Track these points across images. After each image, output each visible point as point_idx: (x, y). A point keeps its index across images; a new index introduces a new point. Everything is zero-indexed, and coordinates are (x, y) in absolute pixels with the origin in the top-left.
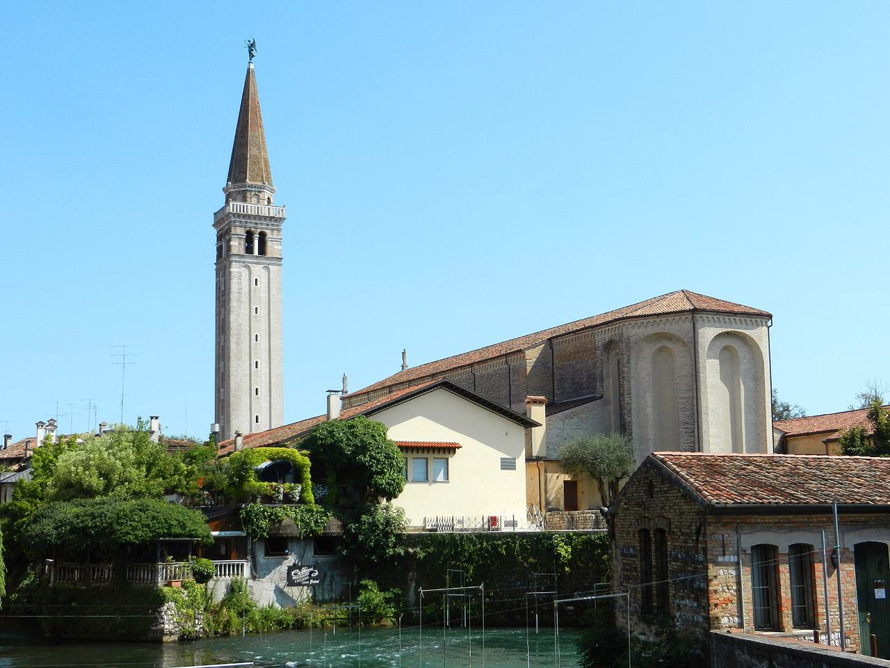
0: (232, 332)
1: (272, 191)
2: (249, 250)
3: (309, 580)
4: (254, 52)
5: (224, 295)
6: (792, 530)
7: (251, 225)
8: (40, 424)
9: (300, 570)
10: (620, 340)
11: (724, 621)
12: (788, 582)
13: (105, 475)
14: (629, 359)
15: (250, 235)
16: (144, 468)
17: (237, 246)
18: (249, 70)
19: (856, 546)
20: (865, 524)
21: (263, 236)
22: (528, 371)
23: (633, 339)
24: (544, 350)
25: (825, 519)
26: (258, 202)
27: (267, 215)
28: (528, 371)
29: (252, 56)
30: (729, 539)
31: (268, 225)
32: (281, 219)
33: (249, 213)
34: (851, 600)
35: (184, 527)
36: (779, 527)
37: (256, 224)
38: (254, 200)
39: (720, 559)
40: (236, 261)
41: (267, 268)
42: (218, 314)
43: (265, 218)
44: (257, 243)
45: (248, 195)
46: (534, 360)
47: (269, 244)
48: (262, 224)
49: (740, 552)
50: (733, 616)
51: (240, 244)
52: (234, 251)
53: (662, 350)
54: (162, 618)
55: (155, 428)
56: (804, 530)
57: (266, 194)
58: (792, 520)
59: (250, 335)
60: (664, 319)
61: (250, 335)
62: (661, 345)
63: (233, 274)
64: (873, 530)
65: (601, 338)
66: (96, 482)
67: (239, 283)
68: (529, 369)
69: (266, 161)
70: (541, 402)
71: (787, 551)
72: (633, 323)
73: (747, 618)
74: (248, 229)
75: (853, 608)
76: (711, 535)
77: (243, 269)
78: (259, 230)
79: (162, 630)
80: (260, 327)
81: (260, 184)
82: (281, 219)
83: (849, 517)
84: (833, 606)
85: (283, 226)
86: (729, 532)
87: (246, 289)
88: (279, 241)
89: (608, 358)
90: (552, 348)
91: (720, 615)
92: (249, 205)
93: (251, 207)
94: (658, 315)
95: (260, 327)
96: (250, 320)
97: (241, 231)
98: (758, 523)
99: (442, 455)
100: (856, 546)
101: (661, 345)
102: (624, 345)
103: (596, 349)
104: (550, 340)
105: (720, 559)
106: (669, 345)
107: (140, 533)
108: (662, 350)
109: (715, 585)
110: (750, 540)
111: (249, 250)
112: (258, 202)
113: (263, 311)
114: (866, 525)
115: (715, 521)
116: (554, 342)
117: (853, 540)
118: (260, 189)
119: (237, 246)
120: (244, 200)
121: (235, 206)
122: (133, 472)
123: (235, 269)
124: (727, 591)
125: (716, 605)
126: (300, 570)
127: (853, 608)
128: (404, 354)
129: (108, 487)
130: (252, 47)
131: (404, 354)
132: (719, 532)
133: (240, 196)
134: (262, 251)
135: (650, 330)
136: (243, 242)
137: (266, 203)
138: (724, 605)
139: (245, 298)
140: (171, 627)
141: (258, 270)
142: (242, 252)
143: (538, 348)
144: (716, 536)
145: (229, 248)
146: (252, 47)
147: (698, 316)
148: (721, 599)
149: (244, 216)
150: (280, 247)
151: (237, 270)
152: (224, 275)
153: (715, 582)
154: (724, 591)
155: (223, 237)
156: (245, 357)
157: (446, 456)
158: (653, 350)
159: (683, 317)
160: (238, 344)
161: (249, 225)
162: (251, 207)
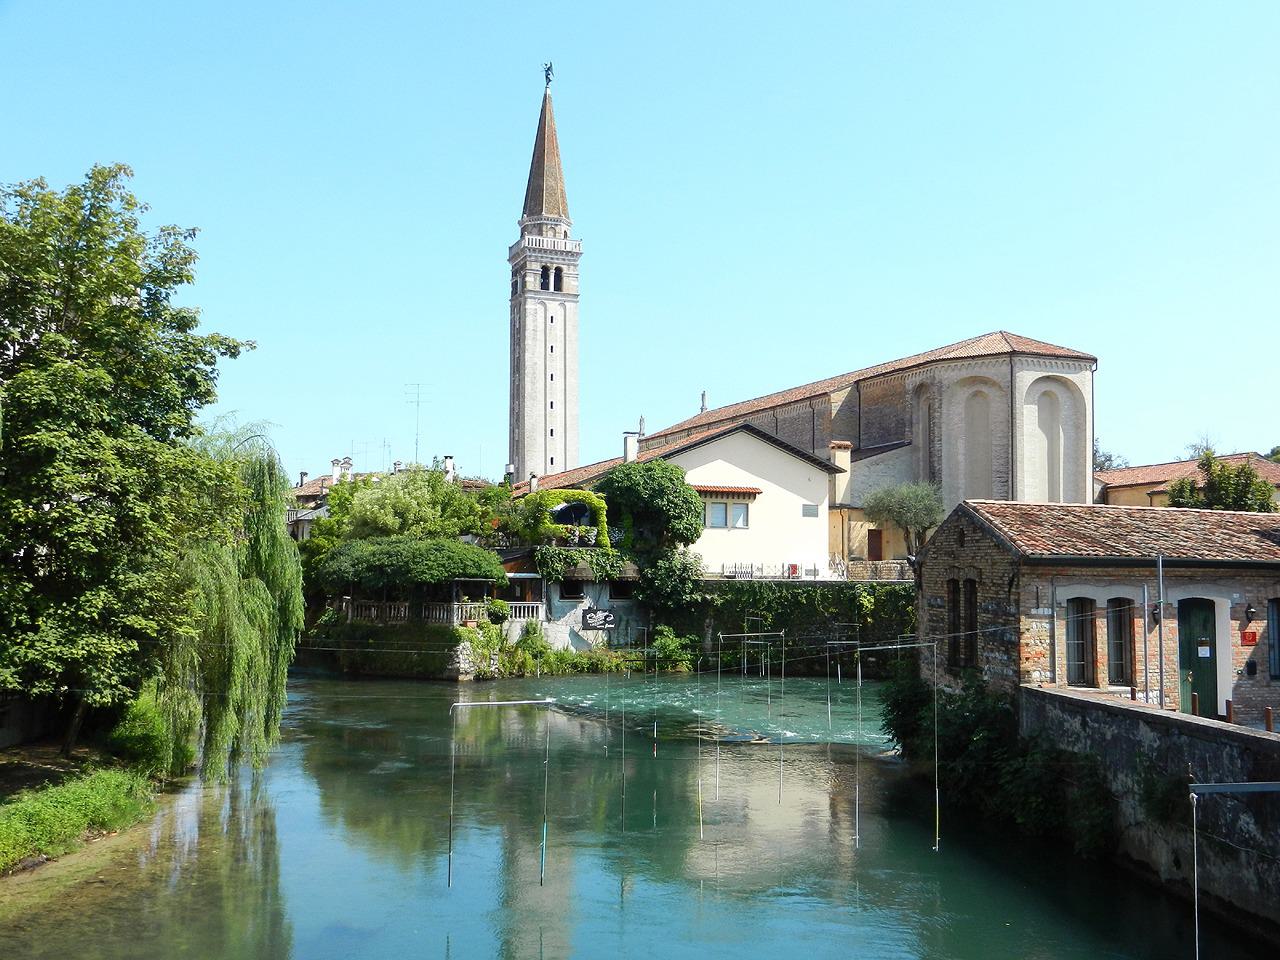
4: (551, 77)
6: (1111, 583)
8: (335, 462)
10: (932, 384)
11: (1035, 675)
13: (400, 514)
15: (545, 270)
16: (439, 508)
17: (533, 281)
18: (545, 95)
21: (559, 271)
22: (833, 415)
23: (945, 382)
24: (850, 395)
25: (1147, 573)
26: (555, 236)
27: (563, 249)
28: (833, 415)
29: (548, 80)
31: (564, 260)
32: (578, 254)
33: (545, 247)
35: (479, 567)
36: (1097, 580)
37: (552, 259)
38: (551, 233)
39: (1033, 611)
40: (531, 298)
41: (562, 304)
42: (513, 351)
43: (562, 252)
44: (553, 279)
45: (544, 229)
46: (840, 403)
47: (565, 280)
48: (557, 259)
49: (1055, 604)
51: (535, 280)
52: (530, 286)
53: (976, 394)
54: (457, 657)
56: (1119, 584)
57: (564, 227)
59: (545, 374)
61: (545, 374)
62: (975, 389)
64: (1200, 586)
65: (912, 381)
66: (392, 521)
67: (535, 321)
68: (834, 413)
69: (562, 192)
70: (846, 448)
72: (946, 366)
77: (539, 306)
78: (555, 266)
81: (556, 216)
82: (578, 254)
85: (580, 261)
86: (1044, 584)
87: (541, 327)
88: (576, 277)
90: (859, 391)
92: (545, 240)
93: (547, 241)
94: (973, 357)
95: (556, 367)
96: (545, 359)
97: (537, 267)
99: (741, 501)
101: (975, 389)
102: (935, 389)
104: (857, 382)
105: (1033, 611)
106: (985, 389)
107: (435, 573)
108: (976, 394)
109: (1028, 638)
110: (1066, 592)
111: (545, 286)
112: (555, 236)
113: (558, 350)
114: (1191, 579)
116: (862, 384)
117: (1177, 595)
118: (557, 222)
119: (533, 281)
120: (540, 233)
121: (531, 239)
122: (428, 512)
123: (531, 305)
125: (1027, 659)
128: (703, 395)
129: (403, 526)
130: (549, 70)
131: (703, 395)
133: (536, 230)
134: (558, 287)
135: (965, 373)
136: (538, 278)
139: (540, 336)
141: (554, 307)
142: (538, 288)
144: (1030, 587)
145: (524, 284)
146: (549, 70)
149: (540, 251)
150: (576, 283)
151: (533, 307)
153: (1027, 635)
155: (519, 271)
158: (967, 395)
159: (1001, 360)
160: (533, 383)
161: (544, 260)
162: (547, 241)
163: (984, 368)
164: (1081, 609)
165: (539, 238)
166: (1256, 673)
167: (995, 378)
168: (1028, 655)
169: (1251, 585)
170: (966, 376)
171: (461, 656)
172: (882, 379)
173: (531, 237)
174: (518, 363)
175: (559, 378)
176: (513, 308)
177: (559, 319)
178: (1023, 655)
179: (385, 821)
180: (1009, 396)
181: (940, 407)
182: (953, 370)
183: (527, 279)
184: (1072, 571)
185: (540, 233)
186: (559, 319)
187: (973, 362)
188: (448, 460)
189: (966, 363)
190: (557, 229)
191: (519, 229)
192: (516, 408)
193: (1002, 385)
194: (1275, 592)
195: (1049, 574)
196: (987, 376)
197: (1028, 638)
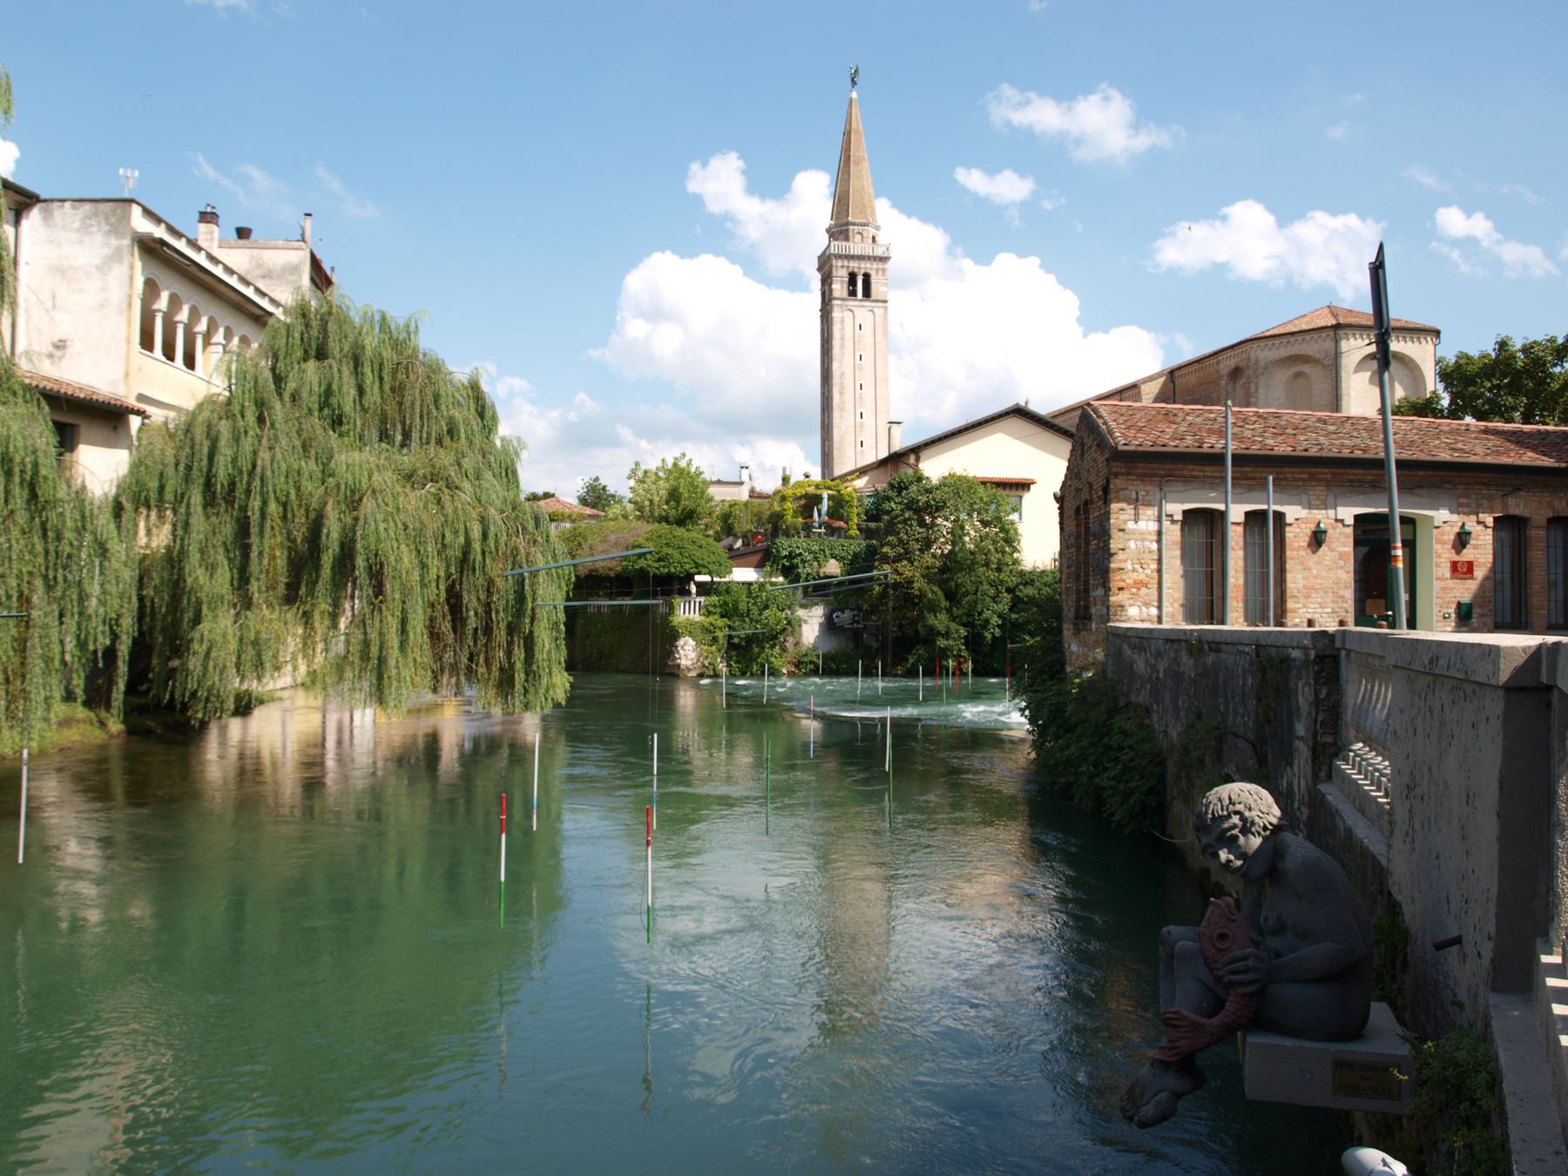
0: (834, 381)
1: (878, 228)
2: (853, 293)
3: (852, 624)
5: (828, 342)
7: (854, 265)
8: (629, 478)
9: (843, 613)
11: (1133, 611)
12: (1241, 563)
14: (1257, 388)
15: (852, 278)
17: (839, 288)
19: (1357, 517)
20: (1374, 486)
21: (867, 277)
23: (1262, 363)
25: (1305, 476)
27: (871, 254)
30: (1146, 498)
33: (852, 253)
34: (1342, 593)
42: (823, 363)
44: (860, 286)
47: (874, 286)
49: (1164, 518)
50: (1147, 605)
52: (836, 294)
53: (1298, 375)
54: (678, 652)
55: (745, 478)
58: (1250, 475)
60: (1300, 338)
62: (1296, 370)
63: (835, 319)
65: (1226, 365)
67: (843, 329)
71: (1241, 519)
73: (1171, 609)
74: (851, 270)
75: (1345, 605)
76: (1117, 492)
78: (862, 271)
79: (679, 666)
80: (866, 378)
81: (865, 221)
83: (1348, 474)
84: (1313, 601)
85: (889, 265)
86: (1148, 488)
87: (849, 334)
89: (1234, 389)
90: (1173, 382)
91: (1126, 603)
93: (856, 246)
94: (1292, 334)
95: (866, 378)
98: (1195, 477)
99: (1014, 492)
100: (1357, 517)
101: (1296, 370)
102: (1251, 371)
103: (1221, 377)
106: (1306, 369)
108: (1298, 375)
109: (1121, 561)
111: (853, 293)
115: (1123, 470)
116: (1177, 374)
119: (839, 288)
120: (847, 239)
121: (838, 246)
123: (836, 314)
124: (1141, 570)
125: (1121, 589)
126: (843, 613)
127: (1345, 605)
132: (1131, 487)
133: (842, 237)
134: (867, 293)
135: (1284, 352)
136: (846, 285)
137: (870, 241)
138: (1134, 590)
139: (849, 345)
140: (689, 663)
142: (845, 294)
143: (1156, 381)
145: (831, 290)
147: (1341, 333)
148: (1130, 581)
152: (827, 322)
153: (1121, 556)
154: (1134, 570)
155: (826, 280)
156: (849, 406)
157: (1019, 493)
158: (1286, 376)
159: (1324, 335)
160: (841, 394)
163: (1297, 346)
164: (1205, 525)
165: (844, 243)
166: (1471, 618)
167: (1317, 356)
168: (1122, 584)
169: (1467, 497)
170: (1285, 355)
171: (681, 652)
172: (1197, 366)
173: (836, 243)
174: (828, 373)
175: (868, 391)
176: (822, 317)
177: (868, 328)
178: (1114, 585)
179: (200, 768)
180: (1334, 375)
181: (1256, 392)
182: (1270, 349)
183: (834, 286)
184: (1189, 470)
185: (847, 239)
186: (868, 328)
187: (1292, 339)
188: (744, 470)
189: (1284, 340)
190: (865, 234)
191: (827, 236)
192: (826, 419)
193: (1326, 362)
194: (1505, 506)
195: (1156, 475)
196: (1308, 353)
197: (1121, 561)
